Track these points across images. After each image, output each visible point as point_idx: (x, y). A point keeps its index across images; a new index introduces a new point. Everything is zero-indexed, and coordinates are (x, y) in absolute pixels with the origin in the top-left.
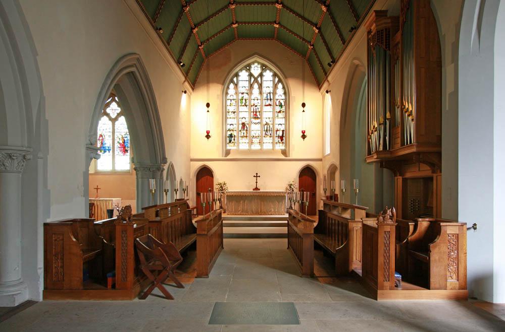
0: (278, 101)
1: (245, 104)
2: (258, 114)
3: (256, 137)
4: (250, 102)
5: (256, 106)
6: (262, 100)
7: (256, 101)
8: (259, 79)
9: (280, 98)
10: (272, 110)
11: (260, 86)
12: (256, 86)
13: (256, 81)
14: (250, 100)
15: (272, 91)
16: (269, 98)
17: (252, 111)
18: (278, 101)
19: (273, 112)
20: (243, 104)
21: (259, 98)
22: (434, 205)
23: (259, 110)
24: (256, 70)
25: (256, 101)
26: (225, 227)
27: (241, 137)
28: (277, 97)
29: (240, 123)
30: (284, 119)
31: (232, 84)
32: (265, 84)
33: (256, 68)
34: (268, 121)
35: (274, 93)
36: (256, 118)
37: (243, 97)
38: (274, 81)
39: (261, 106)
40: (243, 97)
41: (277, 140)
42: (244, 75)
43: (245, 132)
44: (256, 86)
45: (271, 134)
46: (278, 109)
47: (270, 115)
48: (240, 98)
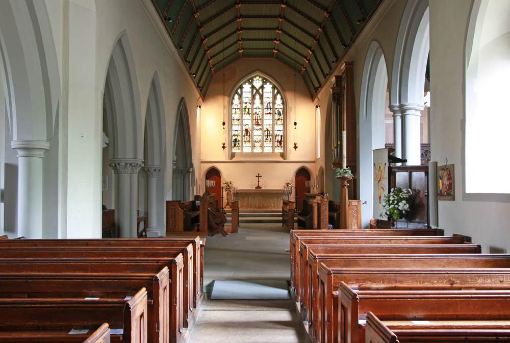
1: (248, 112)
2: (259, 121)
4: (252, 111)
5: (258, 114)
6: (263, 109)
8: (260, 91)
10: (271, 118)
11: (262, 97)
12: (257, 97)
13: (257, 93)
14: (252, 109)
15: (271, 101)
16: (269, 107)
20: (246, 113)
24: (258, 83)
29: (244, 129)
32: (265, 95)
34: (268, 127)
35: (274, 103)
37: (246, 106)
38: (273, 92)
40: (246, 106)
41: (276, 144)
43: (248, 137)
44: (257, 97)
45: (271, 139)
46: (277, 117)
47: (270, 122)
48: (244, 107)
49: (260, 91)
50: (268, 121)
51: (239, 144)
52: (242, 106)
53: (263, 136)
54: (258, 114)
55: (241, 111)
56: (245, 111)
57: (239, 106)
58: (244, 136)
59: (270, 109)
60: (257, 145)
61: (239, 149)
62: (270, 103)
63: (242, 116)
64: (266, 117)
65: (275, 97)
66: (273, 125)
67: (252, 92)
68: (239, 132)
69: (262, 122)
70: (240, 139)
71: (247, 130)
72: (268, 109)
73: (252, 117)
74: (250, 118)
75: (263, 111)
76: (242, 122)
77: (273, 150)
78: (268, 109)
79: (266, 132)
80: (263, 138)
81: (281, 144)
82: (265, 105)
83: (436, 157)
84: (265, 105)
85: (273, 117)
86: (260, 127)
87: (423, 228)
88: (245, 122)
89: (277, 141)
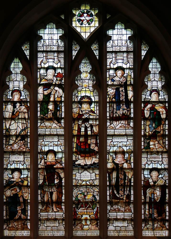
0: (149, 106)
1: (54, 114)
2: (92, 141)
3: (87, 203)
4: (69, 110)
5: (87, 120)
6: (102, 104)
7: (85, 107)
8: (95, 47)
9: (154, 97)
10: (130, 131)
11: (99, 70)
12: (85, 68)
13: (86, 52)
14: (69, 102)
15: (131, 80)
16: (122, 98)
17: (75, 133)
18: (149, 106)
19: (136, 136)
20: (50, 115)
21: (95, 98)
22: (145, 154)
23: (96, 129)
24: (85, 26)
25: (85, 107)
26: (166, 133)
27: (43, 203)
28: (145, 96)
29: (41, 164)
30: (24, 170)
31: (16, 60)
32: (112, 62)
33: (85, 17)
34: (119, 159)
35: (139, 85)
36: (86, 152)
37: (49, 95)
38: (136, 52)
39: (102, 120)
40: (49, 95)
41: (145, 211)
42: (51, 36)
43: (54, 190)
44: (85, 68)
45: (129, 196)
46: (147, 128)
47: (126, 144)
48: (40, 97)
49: (95, 47)
50: (120, 139)
51: (24, 211)
52: (34, 94)
53: (102, 188)
54: (87, 120)
55: (32, 110)
56: (45, 110)
57: (25, 95)
58: (41, 187)
59: (128, 102)
60: (85, 214)
61: (24, 228)
62: (125, 85)
63: (34, 128)
64: (116, 128)
65: (141, 69)
66: (137, 152)
67: (67, 52)
68: (25, 174)
69: (102, 145)
70: (27, 196)
71: (50, 169)
72: (119, 103)
73: (68, 128)
74: (61, 131)
75: (103, 111)
76: (35, 144)
77: (138, 230)
78: (119, 103)
79: (114, 175)
80: (102, 193)
81: (161, 212)
82: (111, 91)
83: (42, 200)
84: (111, 91)
85: (137, 128)
86: (95, 160)
87: (25, 235)
88: (46, 145)
89: (150, 203)
